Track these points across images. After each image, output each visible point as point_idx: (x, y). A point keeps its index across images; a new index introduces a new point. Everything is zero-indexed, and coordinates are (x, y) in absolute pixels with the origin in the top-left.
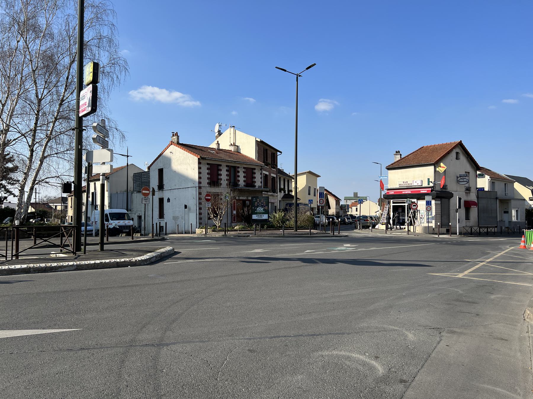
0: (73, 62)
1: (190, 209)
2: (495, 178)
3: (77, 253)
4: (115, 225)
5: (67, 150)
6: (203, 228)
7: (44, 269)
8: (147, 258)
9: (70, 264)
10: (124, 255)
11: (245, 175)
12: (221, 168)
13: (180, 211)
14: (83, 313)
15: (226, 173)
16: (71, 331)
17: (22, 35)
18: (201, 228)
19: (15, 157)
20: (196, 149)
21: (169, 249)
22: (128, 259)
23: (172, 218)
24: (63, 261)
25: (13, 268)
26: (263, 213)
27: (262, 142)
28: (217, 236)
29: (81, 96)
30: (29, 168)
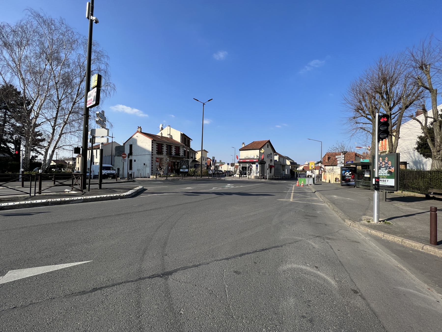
0: (81, 82)
1: (146, 166)
2: (280, 156)
3: (83, 190)
4: (105, 173)
5: (77, 131)
6: (154, 175)
7: (59, 202)
8: (130, 193)
9: (79, 199)
10: (115, 192)
11: (175, 150)
12: (163, 145)
13: (141, 166)
14: (91, 241)
15: (166, 148)
16: (82, 264)
17: (48, 60)
18: (153, 175)
19: (43, 133)
20: (150, 135)
21: (141, 187)
22: (118, 195)
23: (137, 170)
24: (73, 196)
25: (35, 202)
26: (185, 169)
27: (184, 134)
28: (162, 180)
29: (88, 95)
30: (52, 139)
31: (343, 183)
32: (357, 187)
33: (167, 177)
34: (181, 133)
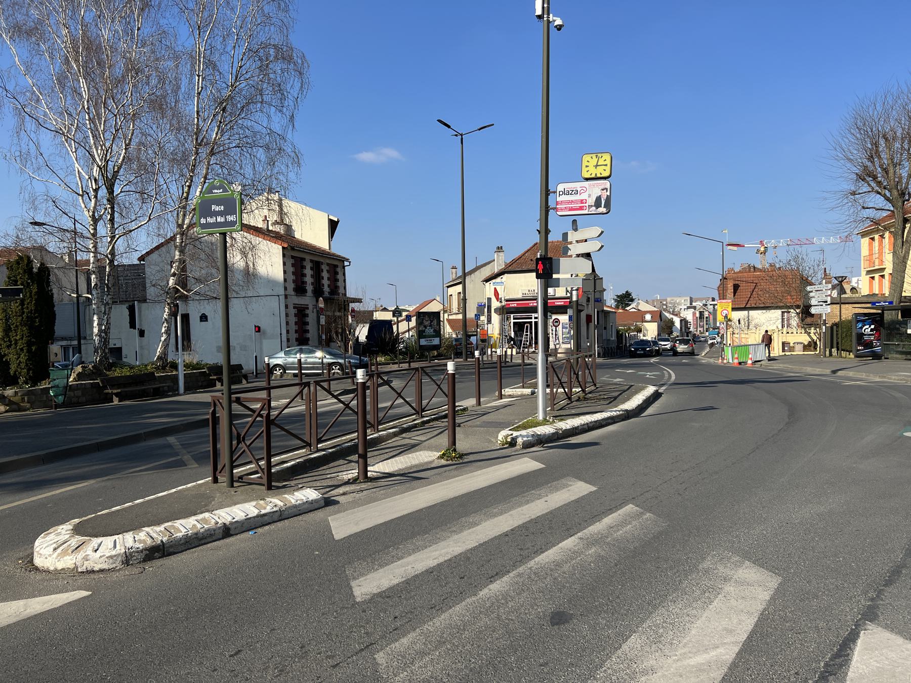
1: (264, 333)
31: (858, 350)
32: (885, 358)
33: (409, 362)
34: (332, 217)
